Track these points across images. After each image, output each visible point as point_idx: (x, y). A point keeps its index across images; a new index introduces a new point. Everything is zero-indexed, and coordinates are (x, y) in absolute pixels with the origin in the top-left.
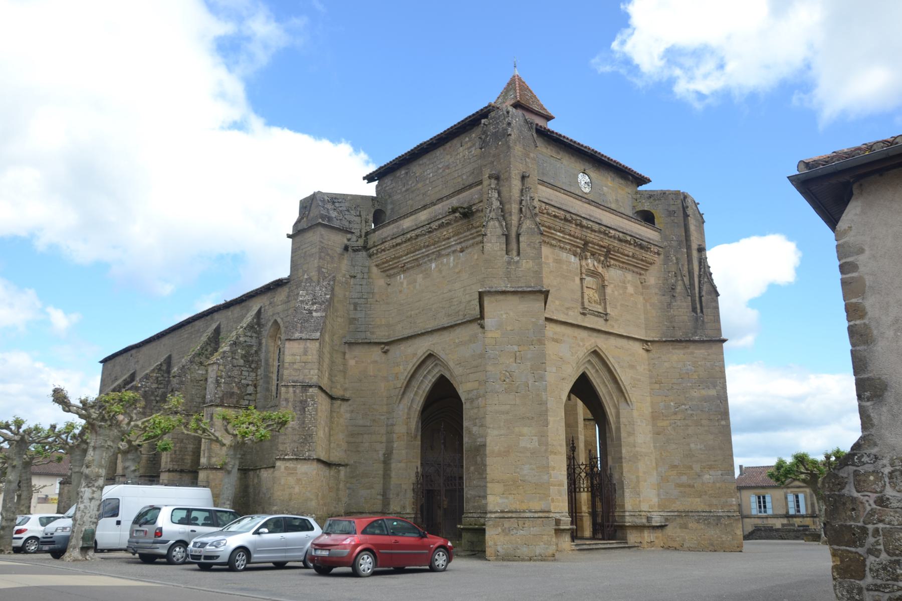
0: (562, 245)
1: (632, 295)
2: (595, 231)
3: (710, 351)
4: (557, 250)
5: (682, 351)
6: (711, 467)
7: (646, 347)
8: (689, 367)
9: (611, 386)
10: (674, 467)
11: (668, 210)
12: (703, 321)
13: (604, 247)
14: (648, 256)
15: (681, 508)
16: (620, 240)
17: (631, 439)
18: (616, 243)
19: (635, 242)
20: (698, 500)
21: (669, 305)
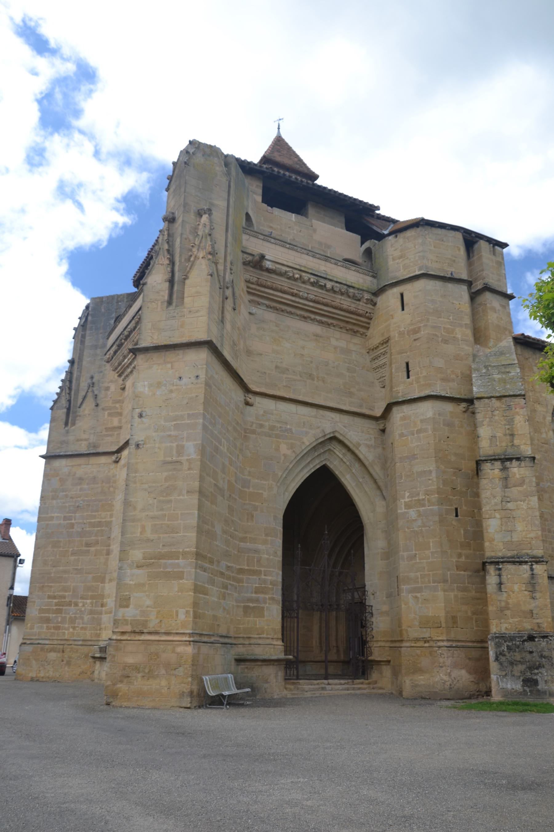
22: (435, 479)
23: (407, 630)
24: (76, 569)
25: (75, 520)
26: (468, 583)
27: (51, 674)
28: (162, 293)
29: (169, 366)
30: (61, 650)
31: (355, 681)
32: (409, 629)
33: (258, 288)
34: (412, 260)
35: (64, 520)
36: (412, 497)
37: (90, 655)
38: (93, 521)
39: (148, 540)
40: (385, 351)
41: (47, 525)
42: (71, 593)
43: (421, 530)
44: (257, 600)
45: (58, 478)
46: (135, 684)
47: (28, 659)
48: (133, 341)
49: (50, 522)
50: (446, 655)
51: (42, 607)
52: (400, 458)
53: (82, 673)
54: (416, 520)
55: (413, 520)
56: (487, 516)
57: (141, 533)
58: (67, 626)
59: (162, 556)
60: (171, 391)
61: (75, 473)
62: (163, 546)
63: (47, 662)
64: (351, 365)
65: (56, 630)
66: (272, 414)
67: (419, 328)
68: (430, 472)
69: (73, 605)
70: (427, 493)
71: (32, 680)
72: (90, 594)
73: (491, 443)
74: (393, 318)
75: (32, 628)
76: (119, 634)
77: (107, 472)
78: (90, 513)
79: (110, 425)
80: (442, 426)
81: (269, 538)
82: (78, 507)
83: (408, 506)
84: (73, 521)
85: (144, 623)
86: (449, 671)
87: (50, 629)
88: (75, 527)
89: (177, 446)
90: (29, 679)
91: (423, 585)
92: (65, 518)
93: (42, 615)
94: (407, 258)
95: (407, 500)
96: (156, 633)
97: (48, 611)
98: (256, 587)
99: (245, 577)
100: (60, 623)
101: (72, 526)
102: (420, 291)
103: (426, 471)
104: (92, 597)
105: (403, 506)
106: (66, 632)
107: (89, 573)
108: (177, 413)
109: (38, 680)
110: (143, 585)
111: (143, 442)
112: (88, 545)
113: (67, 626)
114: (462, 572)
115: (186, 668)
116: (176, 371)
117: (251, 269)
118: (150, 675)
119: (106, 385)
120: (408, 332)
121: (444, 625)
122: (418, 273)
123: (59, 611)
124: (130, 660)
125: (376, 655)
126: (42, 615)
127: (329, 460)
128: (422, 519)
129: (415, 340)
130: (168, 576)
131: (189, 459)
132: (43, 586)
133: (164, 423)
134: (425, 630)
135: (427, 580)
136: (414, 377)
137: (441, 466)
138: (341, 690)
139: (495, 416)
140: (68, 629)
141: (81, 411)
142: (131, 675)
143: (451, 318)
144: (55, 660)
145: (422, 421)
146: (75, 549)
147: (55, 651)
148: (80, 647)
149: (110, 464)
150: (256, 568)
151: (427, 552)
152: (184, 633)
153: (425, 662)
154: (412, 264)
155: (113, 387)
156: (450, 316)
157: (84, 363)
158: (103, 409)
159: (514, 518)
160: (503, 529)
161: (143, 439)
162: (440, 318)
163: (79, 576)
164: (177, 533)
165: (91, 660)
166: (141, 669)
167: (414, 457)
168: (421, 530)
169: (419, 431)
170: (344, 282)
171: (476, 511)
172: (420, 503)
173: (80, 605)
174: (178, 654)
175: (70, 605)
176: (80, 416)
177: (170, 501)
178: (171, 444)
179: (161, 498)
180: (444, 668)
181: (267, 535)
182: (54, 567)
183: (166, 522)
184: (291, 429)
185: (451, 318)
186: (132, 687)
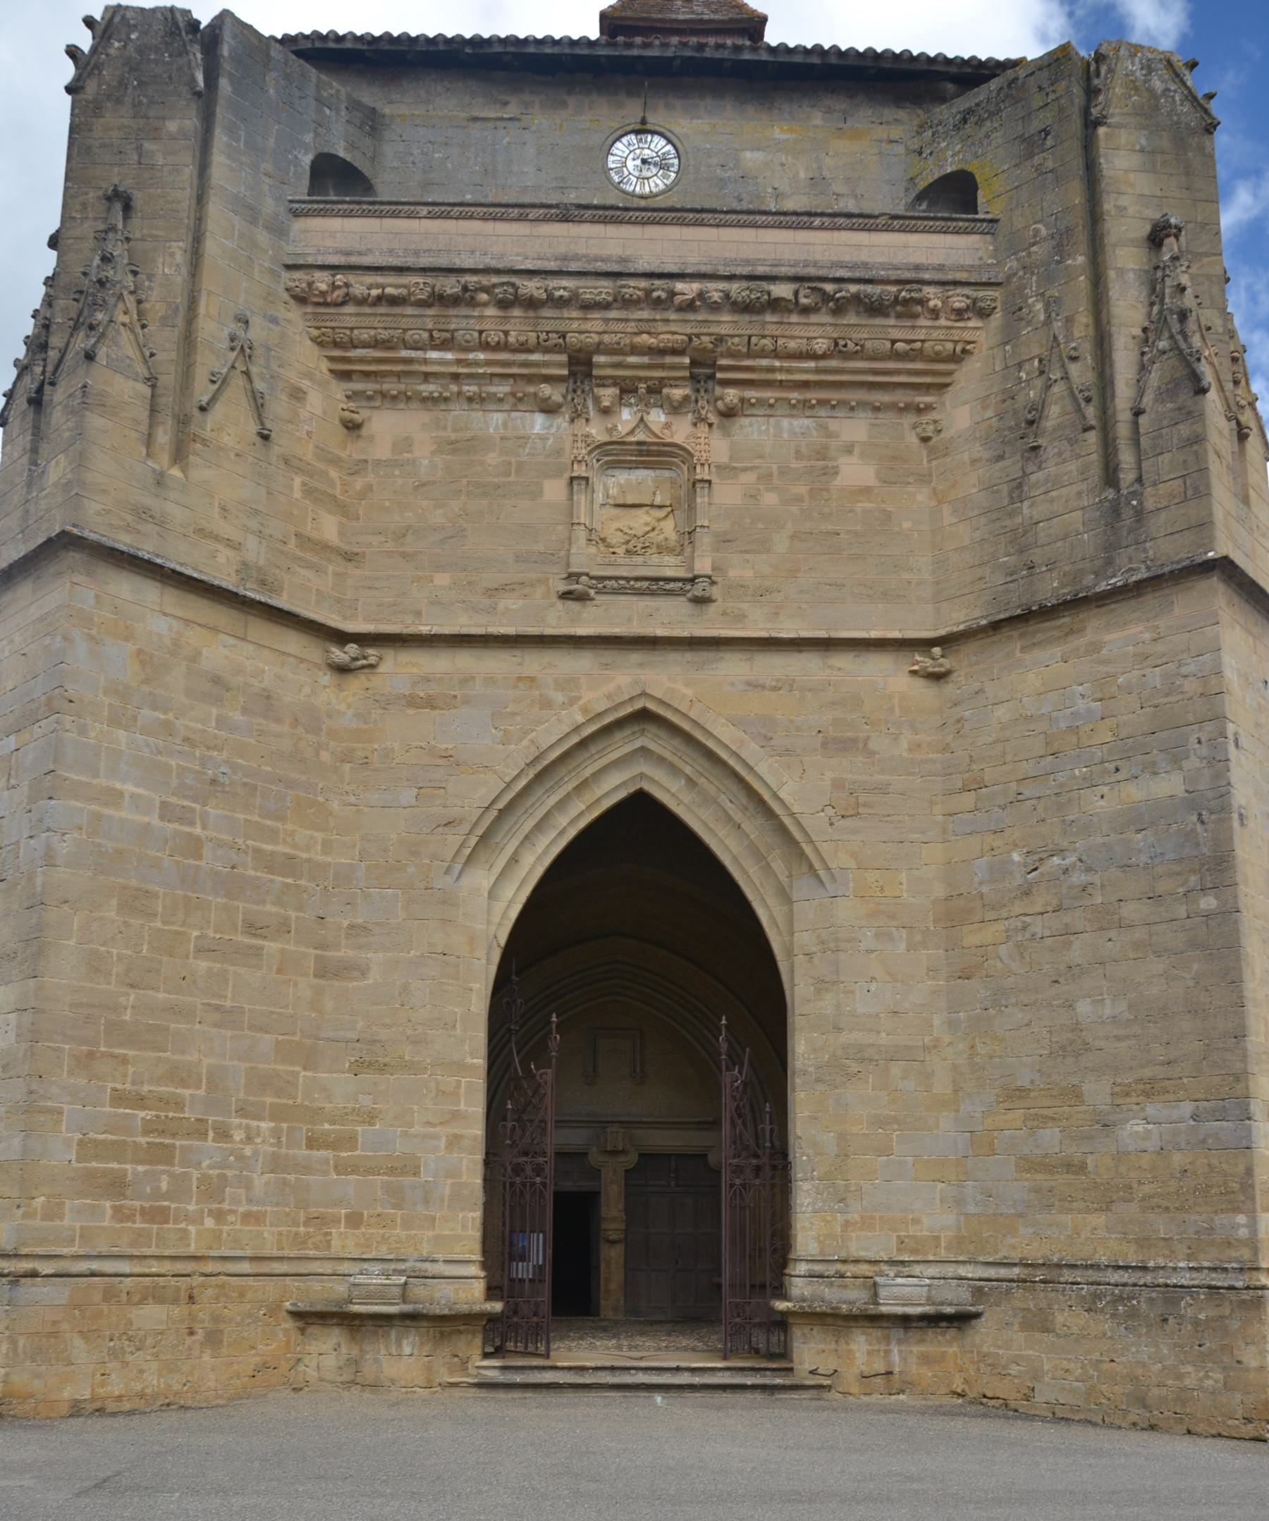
0: (470, 389)
1: (866, 491)
2: (606, 306)
3: (1161, 623)
4: (458, 412)
5: (1057, 651)
6: (1151, 1089)
7: (921, 661)
8: (1081, 705)
9: (753, 826)
10: (1014, 1095)
11: (1022, 139)
12: (1139, 513)
13: (675, 352)
14: (930, 333)
15: (1036, 1252)
16: (746, 308)
17: (827, 1004)
18: (726, 323)
19: (827, 297)
20: (1099, 1220)
21: (1018, 489)
24: (218, 1008)
25: (204, 827)
27: (152, 1381)
30: (183, 1295)
35: (162, 818)
37: (287, 1305)
38: (268, 847)
41: (98, 817)
42: (202, 1092)
45: (131, 647)
47: (54, 1334)
49: (107, 811)
51: (92, 1135)
58: (191, 1208)
65: (152, 1221)
69: (211, 1134)
71: (76, 1410)
72: (269, 1100)
75: (52, 1213)
77: (307, 690)
78: (256, 818)
82: (213, 782)
84: (198, 830)
87: (131, 1218)
90: (65, 1410)
93: (94, 1164)
97: (117, 1150)
100: (168, 1196)
101: (194, 847)
104: (278, 1114)
106: (192, 1229)
107: (264, 1029)
109: (100, 1411)
112: (252, 928)
123: (162, 1155)
126: (94, 1164)
132: (91, 1055)
146: (211, 933)
147: (161, 1300)
148: (250, 1281)
163: (229, 1033)
165: (289, 1324)
173: (238, 1136)
175: (203, 1135)
176: (205, 442)
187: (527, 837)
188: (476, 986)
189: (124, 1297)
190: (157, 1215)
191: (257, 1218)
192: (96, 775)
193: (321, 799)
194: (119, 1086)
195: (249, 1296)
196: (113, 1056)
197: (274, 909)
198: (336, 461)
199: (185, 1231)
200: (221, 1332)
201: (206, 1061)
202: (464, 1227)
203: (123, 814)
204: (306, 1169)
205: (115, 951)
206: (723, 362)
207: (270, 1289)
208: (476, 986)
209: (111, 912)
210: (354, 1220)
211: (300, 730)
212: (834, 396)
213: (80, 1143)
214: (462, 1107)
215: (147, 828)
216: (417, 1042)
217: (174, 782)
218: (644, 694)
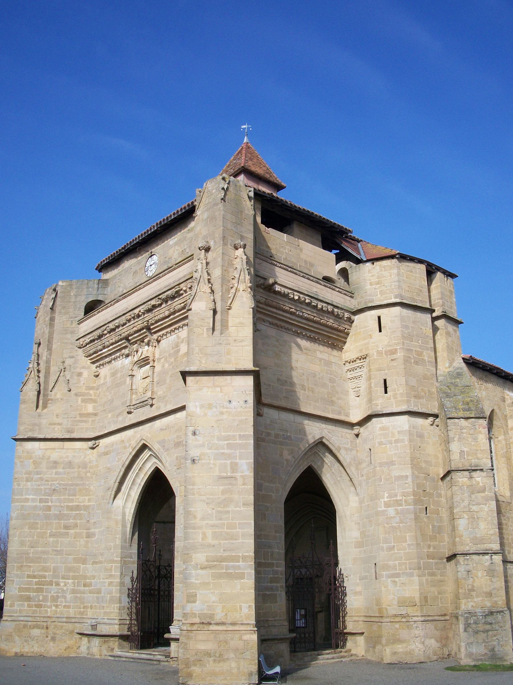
18: (148, 316)
22: (411, 484)
23: (386, 609)
24: (56, 550)
25: (52, 503)
26: (435, 569)
28: (207, 320)
29: (218, 389)
30: (45, 627)
31: (336, 650)
32: (388, 607)
33: (265, 307)
34: (388, 288)
35: (40, 502)
36: (391, 498)
39: (210, 546)
40: (362, 366)
41: (23, 506)
42: (51, 573)
43: (399, 525)
44: (271, 589)
45: (31, 461)
46: (208, 666)
47: (11, 636)
48: (121, 335)
50: (421, 628)
52: (380, 463)
53: (68, 647)
54: (394, 517)
55: (392, 517)
56: (458, 517)
57: (202, 539)
59: (223, 559)
60: (222, 413)
61: (50, 457)
62: (224, 550)
63: (30, 638)
64: (332, 376)
66: (276, 423)
67: (396, 350)
68: (407, 477)
69: (54, 584)
70: (404, 494)
72: (71, 574)
73: (460, 456)
74: (371, 338)
76: (189, 625)
77: (83, 457)
79: (84, 412)
80: (415, 437)
81: (278, 534)
82: (54, 490)
83: (387, 505)
84: (50, 504)
85: (212, 616)
86: (423, 640)
87: (32, 607)
88: (52, 509)
89: (231, 463)
91: (401, 572)
92: (41, 501)
94: (384, 285)
95: (386, 500)
96: (223, 624)
97: (28, 590)
98: (271, 577)
99: (262, 569)
101: (49, 508)
102: (396, 316)
103: (403, 476)
104: (74, 578)
105: (383, 505)
106: (49, 610)
108: (229, 434)
110: (208, 584)
111: (198, 458)
112: (66, 527)
113: (49, 604)
114: (431, 560)
115: (253, 653)
116: (226, 395)
117: (262, 290)
118: (220, 658)
119: (78, 370)
120: (386, 352)
121: (418, 604)
122: (394, 300)
123: (40, 590)
124: (202, 647)
125: (350, 627)
127: (314, 461)
128: (399, 517)
129: (392, 360)
130: (230, 576)
131: (243, 476)
132: (22, 566)
133: (217, 442)
134: (402, 608)
135: (404, 567)
136: (392, 393)
137: (416, 472)
138: (330, 659)
139: (463, 433)
140: (50, 607)
141: (52, 395)
142: (203, 659)
143: (420, 342)
144: (39, 636)
145: (399, 432)
147: (39, 628)
148: (64, 624)
149: (86, 449)
150: (270, 561)
151: (404, 544)
152: (248, 624)
153: (404, 634)
154: (388, 291)
155: (85, 374)
156: (419, 340)
157: (54, 346)
158: (76, 395)
159: (478, 518)
160: (470, 527)
161: (198, 455)
162: (412, 341)
163: (59, 557)
164: (237, 539)
166: (212, 654)
167: (392, 463)
168: (399, 525)
169: (397, 441)
170: (330, 302)
171: (440, 509)
172: (398, 503)
173: (62, 584)
174: (245, 641)
176: (52, 400)
177: (228, 512)
178: (225, 461)
179: (219, 509)
180: (418, 638)
181: (276, 532)
182: (32, 547)
183: (225, 530)
184: (290, 436)
185: (420, 342)
186: (205, 669)
187: (130, 488)
188: (117, 536)
189: (29, 627)
190: (39, 606)
191: (69, 607)
192: (22, 496)
193: (87, 487)
194: (29, 573)
195: (64, 628)
196: (27, 566)
197: (73, 521)
198: (92, 388)
199: (47, 610)
200: (56, 637)
201: (53, 565)
202: (114, 609)
203: (29, 504)
204: (84, 593)
205: (27, 539)
206: (152, 327)
207: (70, 626)
208: (117, 536)
209: (26, 530)
210: (91, 607)
211: (80, 469)
212: (176, 326)
213: (19, 588)
214: (113, 573)
215: (36, 506)
216: (102, 554)
217: (43, 492)
218: (142, 439)
